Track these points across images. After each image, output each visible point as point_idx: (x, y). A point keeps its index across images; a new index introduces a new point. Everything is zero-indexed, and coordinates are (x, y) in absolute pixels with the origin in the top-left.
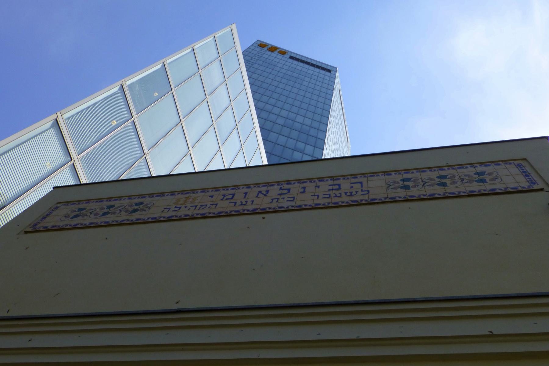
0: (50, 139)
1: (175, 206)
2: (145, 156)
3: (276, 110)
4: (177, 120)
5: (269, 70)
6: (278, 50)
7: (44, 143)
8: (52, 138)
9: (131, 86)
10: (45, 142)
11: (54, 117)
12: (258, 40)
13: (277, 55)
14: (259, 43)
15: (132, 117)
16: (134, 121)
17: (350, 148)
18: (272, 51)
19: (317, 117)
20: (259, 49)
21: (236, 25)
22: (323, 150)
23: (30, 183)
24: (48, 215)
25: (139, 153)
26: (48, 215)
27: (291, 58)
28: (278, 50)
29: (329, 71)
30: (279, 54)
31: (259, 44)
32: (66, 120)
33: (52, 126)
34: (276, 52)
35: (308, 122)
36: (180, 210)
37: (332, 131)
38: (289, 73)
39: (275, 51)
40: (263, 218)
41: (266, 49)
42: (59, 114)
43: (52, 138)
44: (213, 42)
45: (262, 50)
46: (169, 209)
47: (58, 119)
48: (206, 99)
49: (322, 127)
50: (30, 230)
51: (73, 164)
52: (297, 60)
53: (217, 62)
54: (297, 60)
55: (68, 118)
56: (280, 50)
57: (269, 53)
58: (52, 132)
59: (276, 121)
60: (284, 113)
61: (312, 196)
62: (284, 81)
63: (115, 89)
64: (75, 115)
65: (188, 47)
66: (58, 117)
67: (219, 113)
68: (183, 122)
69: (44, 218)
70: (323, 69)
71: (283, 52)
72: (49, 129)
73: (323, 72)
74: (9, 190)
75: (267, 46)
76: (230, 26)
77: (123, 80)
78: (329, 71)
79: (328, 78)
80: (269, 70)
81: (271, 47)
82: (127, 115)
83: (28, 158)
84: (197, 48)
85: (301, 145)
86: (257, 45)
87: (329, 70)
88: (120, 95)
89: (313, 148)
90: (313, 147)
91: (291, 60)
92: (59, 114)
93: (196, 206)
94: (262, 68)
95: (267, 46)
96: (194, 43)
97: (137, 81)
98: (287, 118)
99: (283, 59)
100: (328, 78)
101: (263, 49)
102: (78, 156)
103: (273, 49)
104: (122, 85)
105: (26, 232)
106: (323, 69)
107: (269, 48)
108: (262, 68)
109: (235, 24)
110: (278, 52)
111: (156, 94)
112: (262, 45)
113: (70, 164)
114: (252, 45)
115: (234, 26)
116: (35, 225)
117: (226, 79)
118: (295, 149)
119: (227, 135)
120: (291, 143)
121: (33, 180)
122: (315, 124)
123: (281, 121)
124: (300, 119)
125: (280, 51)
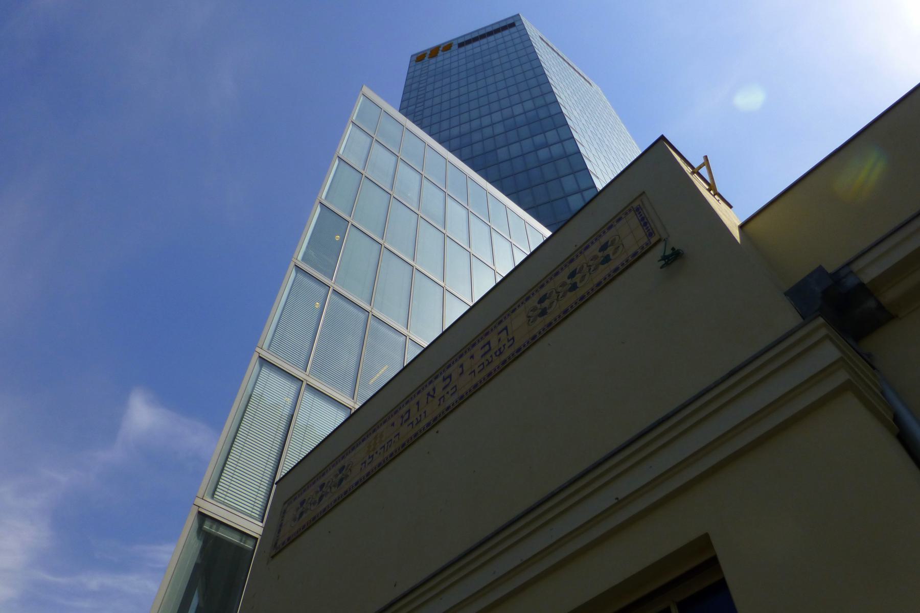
0: (228, 495)
1: (368, 457)
2: (371, 313)
3: (486, 121)
4: (377, 246)
5: (447, 81)
6: (441, 49)
7: (248, 437)
8: (234, 476)
9: (303, 259)
10: (246, 442)
11: (255, 357)
12: (412, 56)
13: (443, 55)
14: (415, 58)
15: (330, 287)
16: (334, 290)
17: (600, 92)
18: (435, 56)
19: (536, 92)
20: (419, 66)
21: (368, 86)
22: (568, 124)
23: (279, 441)
24: (281, 525)
25: (362, 316)
26: (281, 525)
27: (461, 45)
28: (441, 49)
29: (512, 25)
30: (445, 52)
31: (416, 59)
32: (268, 349)
33: (261, 366)
34: (440, 53)
35: (529, 105)
36: (374, 459)
37: (569, 87)
38: (471, 65)
39: (438, 53)
40: (437, 432)
41: (426, 58)
42: (258, 350)
43: (247, 439)
44: (355, 129)
45: (424, 63)
46: (365, 462)
47: (260, 355)
48: (392, 197)
49: (549, 99)
50: (273, 553)
51: (307, 384)
52: (468, 42)
53: (375, 145)
54: (468, 42)
55: (270, 346)
56: (442, 46)
57: (433, 60)
58: (265, 371)
59: (493, 127)
60: (497, 117)
61: (469, 374)
62: (472, 79)
63: (292, 274)
64: (274, 335)
65: (348, 124)
66: (259, 354)
67: (416, 199)
68: (385, 244)
69: (279, 531)
70: (504, 28)
71: (447, 47)
72: (260, 371)
73: (506, 32)
74: (269, 455)
75: (426, 54)
76: (361, 93)
77: (293, 259)
78: (512, 25)
79: (517, 35)
80: (447, 81)
81: (431, 52)
82: (323, 290)
83: (261, 417)
84: (343, 153)
85: (539, 139)
86: (414, 62)
87: (512, 25)
88: (301, 277)
89: (554, 132)
90: (555, 130)
91: (462, 49)
92: (258, 350)
93: (384, 446)
94: (438, 84)
95: (426, 54)
96: (336, 150)
97: (307, 247)
98: (503, 120)
99: (455, 53)
100: (517, 35)
101: (423, 61)
102: (306, 372)
103: (434, 52)
104: (296, 265)
105: (273, 557)
106: (504, 28)
107: (430, 54)
108: (438, 84)
109: (364, 86)
110: (442, 51)
111: (338, 237)
112: (420, 58)
113: (304, 386)
114: (409, 67)
115: (366, 90)
116: (276, 544)
117: (398, 155)
118: (537, 149)
119: (442, 213)
120: (527, 145)
121: (284, 426)
122: (539, 102)
123: (499, 129)
124: (518, 110)
125: (443, 48)
